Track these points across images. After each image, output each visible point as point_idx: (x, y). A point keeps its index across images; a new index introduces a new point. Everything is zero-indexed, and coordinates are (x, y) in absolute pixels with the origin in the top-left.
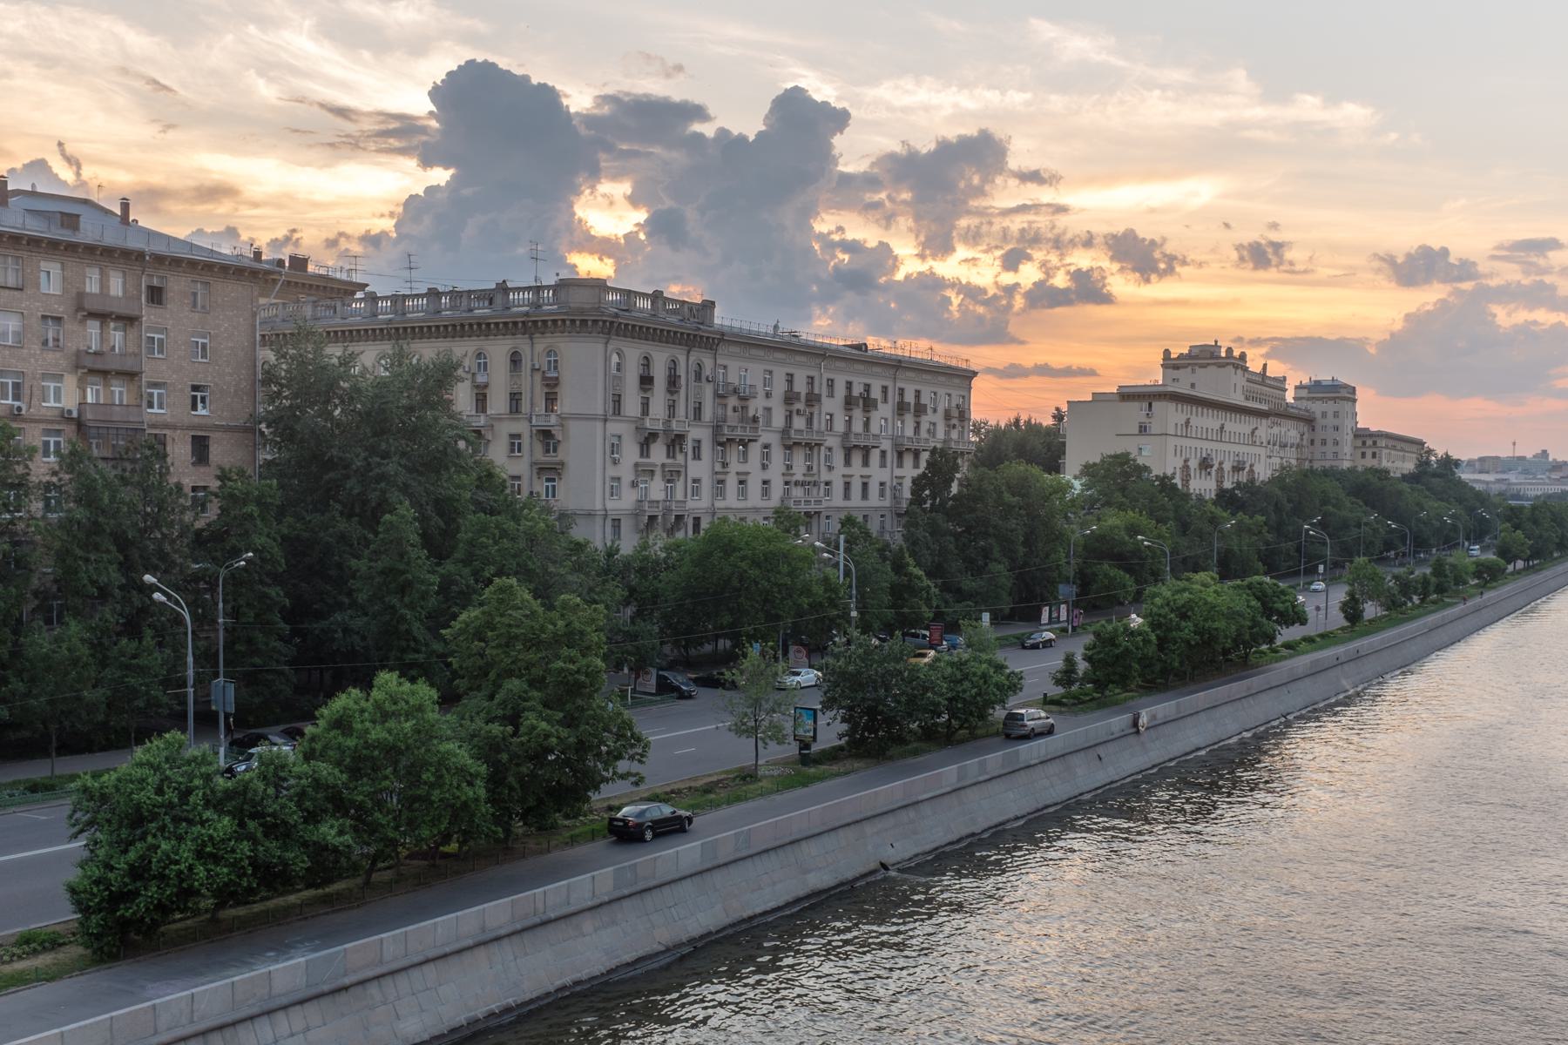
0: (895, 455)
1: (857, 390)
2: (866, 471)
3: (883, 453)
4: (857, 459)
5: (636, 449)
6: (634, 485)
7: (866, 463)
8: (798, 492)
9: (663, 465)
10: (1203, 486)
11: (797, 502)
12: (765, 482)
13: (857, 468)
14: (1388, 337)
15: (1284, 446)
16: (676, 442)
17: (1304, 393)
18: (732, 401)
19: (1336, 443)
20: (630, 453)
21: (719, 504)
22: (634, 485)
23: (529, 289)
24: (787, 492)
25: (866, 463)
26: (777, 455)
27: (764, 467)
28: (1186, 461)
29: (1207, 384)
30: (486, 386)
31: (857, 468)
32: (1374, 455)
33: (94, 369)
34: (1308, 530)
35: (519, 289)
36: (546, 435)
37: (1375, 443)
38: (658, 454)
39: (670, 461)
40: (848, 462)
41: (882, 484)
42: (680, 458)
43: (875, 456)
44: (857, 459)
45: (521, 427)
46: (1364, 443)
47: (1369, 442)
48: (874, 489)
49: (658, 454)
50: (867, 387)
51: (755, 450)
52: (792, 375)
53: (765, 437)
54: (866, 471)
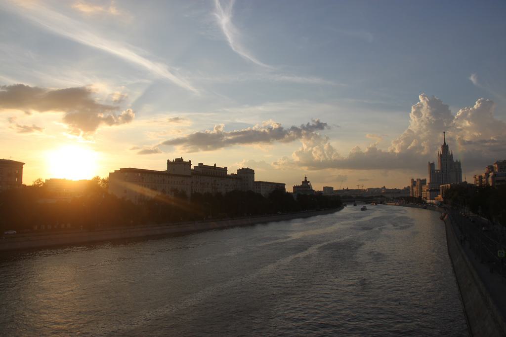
14: (114, 172)
17: (239, 172)
32: (259, 188)
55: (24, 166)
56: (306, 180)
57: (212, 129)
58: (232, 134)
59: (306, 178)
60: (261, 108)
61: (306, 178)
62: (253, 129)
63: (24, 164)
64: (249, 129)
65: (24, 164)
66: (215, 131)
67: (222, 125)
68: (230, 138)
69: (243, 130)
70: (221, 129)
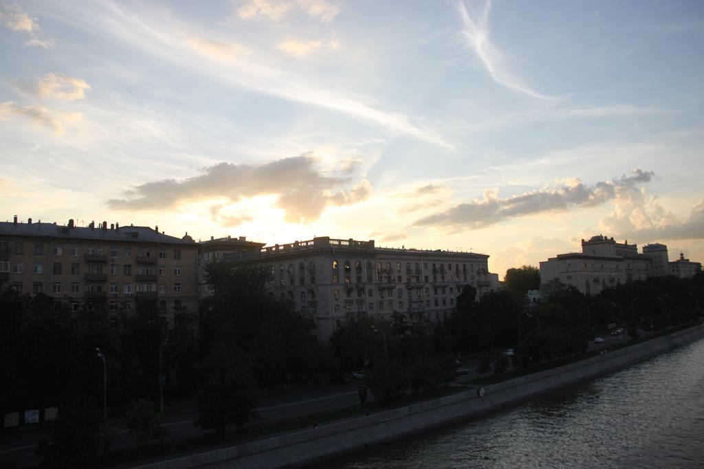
0: (457, 289)
1: (438, 267)
2: (444, 296)
3: (451, 289)
4: (439, 291)
5: (345, 294)
6: (345, 307)
7: (444, 293)
8: (415, 305)
9: (357, 300)
10: (597, 289)
11: (414, 309)
12: (400, 303)
13: (440, 295)
15: (639, 270)
16: (361, 291)
17: (646, 250)
18: (384, 275)
19: (661, 267)
20: (343, 295)
21: (382, 312)
22: (345, 307)
23: (337, 240)
24: (410, 306)
25: (444, 293)
26: (405, 292)
27: (400, 297)
28: (587, 280)
29: (600, 251)
30: (293, 276)
31: (440, 295)
32: (677, 270)
33: (140, 279)
34: (98, 352)
35: (332, 240)
36: (311, 291)
37: (677, 266)
38: (354, 295)
39: (359, 298)
40: (436, 293)
41: (452, 300)
42: (363, 297)
43: (448, 290)
44: (439, 291)
45: (372, 287)
46: (673, 266)
47: (675, 266)
48: (448, 301)
49: (354, 295)
50: (442, 265)
51: (395, 292)
52: (426, 264)
53: (399, 286)
54: (444, 296)
55: (489, 260)
56: (682, 258)
57: (481, 198)
58: (511, 202)
59: (682, 254)
60: (544, 162)
61: (682, 254)
62: (541, 191)
63: (489, 256)
64: (534, 191)
65: (489, 256)
66: (485, 200)
67: (496, 191)
68: (507, 207)
69: (525, 194)
70: (494, 197)
